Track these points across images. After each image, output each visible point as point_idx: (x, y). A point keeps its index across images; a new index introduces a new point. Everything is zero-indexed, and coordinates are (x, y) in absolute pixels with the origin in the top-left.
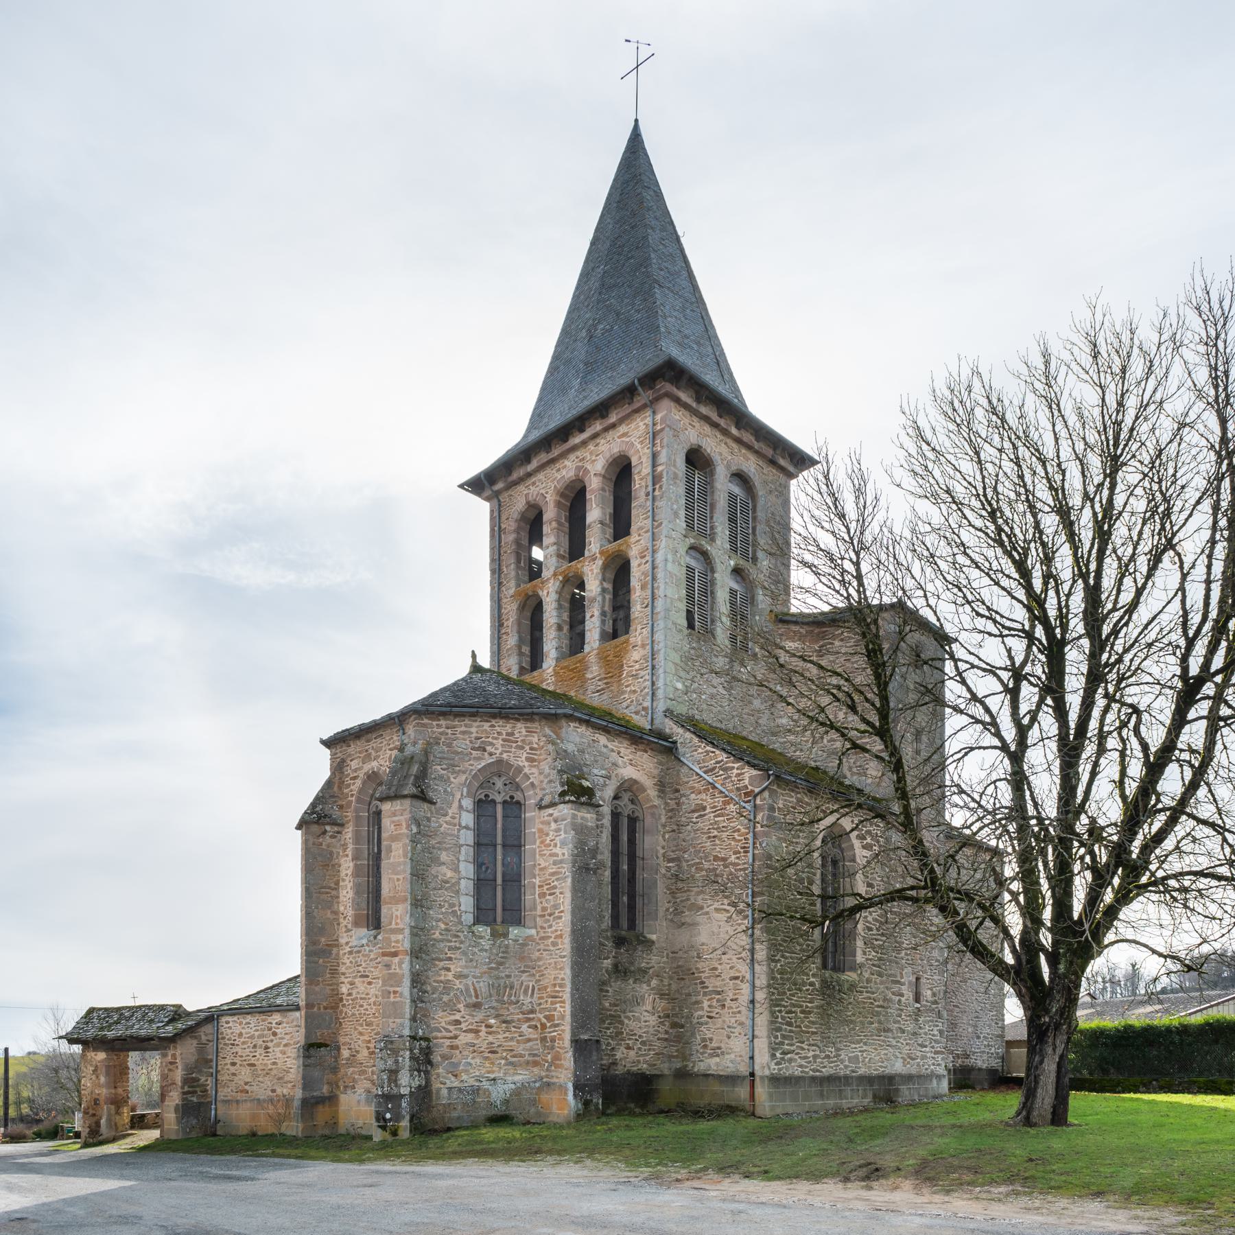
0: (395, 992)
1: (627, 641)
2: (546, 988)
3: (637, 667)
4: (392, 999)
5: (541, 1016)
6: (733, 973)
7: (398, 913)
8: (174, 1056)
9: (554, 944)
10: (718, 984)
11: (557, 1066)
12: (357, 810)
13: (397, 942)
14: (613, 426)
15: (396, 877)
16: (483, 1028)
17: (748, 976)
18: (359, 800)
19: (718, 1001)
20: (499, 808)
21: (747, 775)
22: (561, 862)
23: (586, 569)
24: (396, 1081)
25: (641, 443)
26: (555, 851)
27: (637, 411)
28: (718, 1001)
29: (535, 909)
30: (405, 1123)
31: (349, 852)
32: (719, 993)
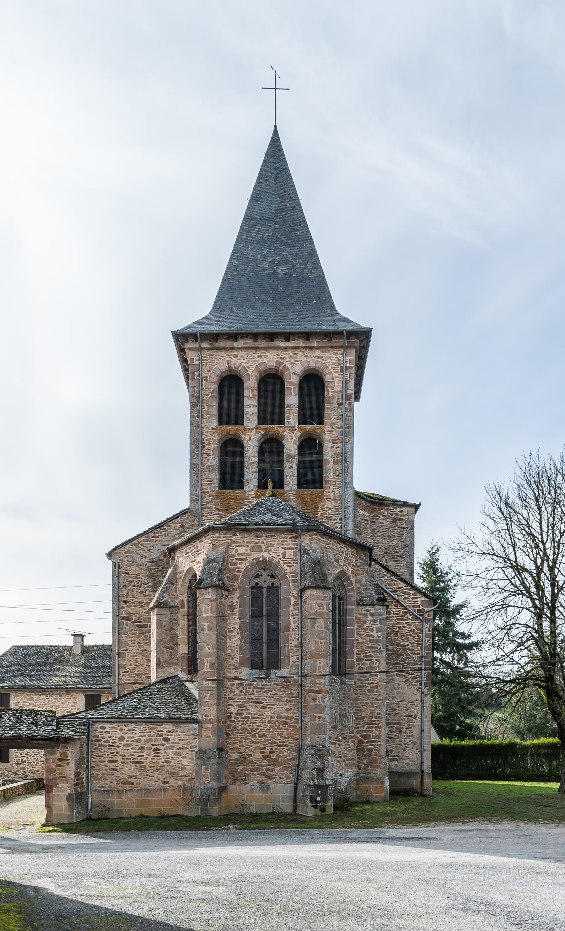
0: (319, 717)
1: (322, 493)
2: (363, 718)
3: (330, 512)
4: (317, 722)
5: (358, 735)
6: (407, 713)
7: (321, 665)
8: (65, 754)
9: (370, 691)
10: (396, 718)
11: (373, 767)
12: (241, 583)
13: (321, 684)
14: (311, 348)
15: (319, 641)
16: (337, 742)
17: (419, 715)
18: (244, 576)
19: (396, 728)
20: (265, 591)
21: (419, 600)
22: (377, 641)
23: (287, 434)
24: (322, 776)
25: (334, 369)
26: (371, 633)
27: (332, 347)
28: (396, 728)
29: (353, 668)
30: (330, 803)
31: (237, 611)
32: (397, 724)
